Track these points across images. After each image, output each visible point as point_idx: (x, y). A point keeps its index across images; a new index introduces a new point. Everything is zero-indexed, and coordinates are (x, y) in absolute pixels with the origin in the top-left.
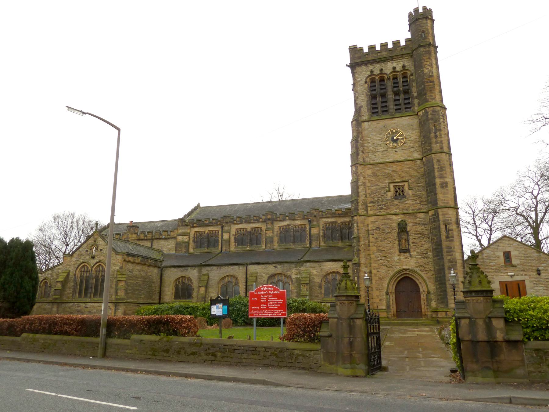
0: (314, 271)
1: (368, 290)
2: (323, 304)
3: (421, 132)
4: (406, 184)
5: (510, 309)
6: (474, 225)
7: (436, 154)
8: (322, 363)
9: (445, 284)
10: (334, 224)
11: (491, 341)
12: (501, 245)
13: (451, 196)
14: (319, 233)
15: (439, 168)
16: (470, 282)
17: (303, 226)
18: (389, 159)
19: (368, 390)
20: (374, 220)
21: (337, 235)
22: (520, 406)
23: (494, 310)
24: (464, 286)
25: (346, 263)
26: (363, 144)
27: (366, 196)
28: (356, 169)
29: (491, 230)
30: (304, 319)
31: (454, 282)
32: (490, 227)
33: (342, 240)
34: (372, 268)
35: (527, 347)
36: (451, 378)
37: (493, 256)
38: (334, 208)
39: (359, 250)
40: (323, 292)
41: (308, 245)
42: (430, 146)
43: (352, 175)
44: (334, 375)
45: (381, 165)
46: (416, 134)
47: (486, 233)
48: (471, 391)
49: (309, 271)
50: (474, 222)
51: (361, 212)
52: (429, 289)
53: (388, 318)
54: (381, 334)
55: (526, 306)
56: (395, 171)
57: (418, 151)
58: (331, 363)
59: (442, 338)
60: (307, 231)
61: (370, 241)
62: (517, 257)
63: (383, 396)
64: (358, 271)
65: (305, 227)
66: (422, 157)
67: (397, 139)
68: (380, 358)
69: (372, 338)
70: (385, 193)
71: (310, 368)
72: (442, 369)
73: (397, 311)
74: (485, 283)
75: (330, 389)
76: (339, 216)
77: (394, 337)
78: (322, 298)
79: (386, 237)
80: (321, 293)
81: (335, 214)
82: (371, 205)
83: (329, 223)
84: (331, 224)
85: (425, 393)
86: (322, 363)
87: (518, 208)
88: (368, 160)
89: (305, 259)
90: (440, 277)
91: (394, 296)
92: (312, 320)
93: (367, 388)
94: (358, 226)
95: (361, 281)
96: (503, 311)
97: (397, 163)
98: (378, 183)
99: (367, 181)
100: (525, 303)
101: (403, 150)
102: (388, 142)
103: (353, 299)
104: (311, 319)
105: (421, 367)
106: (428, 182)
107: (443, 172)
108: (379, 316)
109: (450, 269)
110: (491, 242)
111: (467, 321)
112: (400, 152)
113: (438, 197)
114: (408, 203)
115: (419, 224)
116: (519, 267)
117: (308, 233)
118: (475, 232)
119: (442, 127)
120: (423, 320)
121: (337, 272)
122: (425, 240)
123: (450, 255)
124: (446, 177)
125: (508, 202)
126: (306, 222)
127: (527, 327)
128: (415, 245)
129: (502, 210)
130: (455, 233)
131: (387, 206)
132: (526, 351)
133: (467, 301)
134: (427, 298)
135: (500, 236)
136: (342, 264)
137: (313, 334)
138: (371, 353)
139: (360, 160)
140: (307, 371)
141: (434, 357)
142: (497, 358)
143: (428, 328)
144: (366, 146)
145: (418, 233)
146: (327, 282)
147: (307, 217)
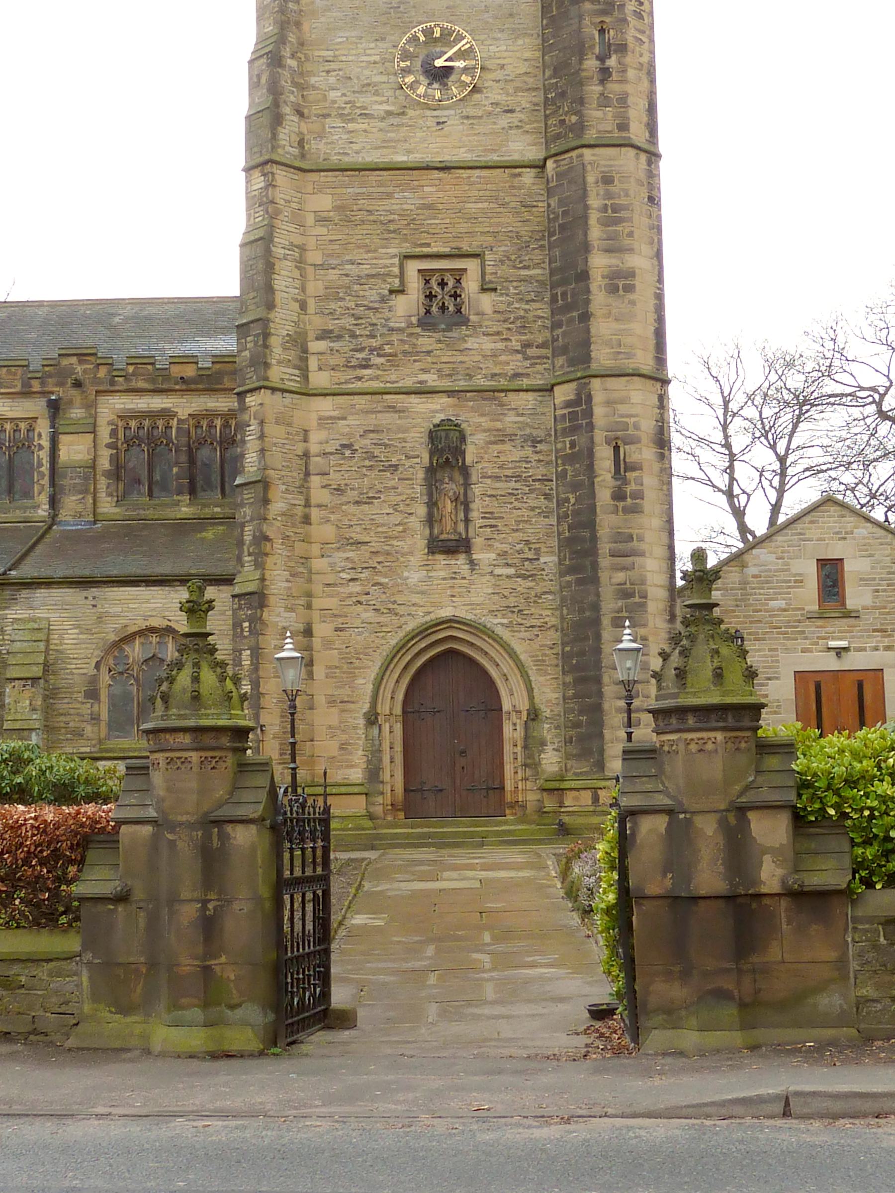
0: (67, 625)
1: (295, 707)
2: (101, 764)
3: (545, 49)
4: (472, 265)
5: (815, 775)
6: (723, 450)
7: (597, 151)
8: (87, 1008)
9: (598, 681)
10: (160, 423)
11: (741, 896)
12: (813, 532)
13: (644, 329)
14: (94, 460)
15: (605, 208)
16: (681, 674)
17: (23, 426)
18: (408, 152)
19: (269, 1106)
20: (335, 413)
21: (175, 470)
22: (817, 1124)
23: (760, 779)
24: (659, 688)
25: (201, 590)
26: (301, 74)
27: (303, 306)
28: (266, 188)
29: (783, 474)
30: (12, 827)
31: (632, 672)
32: (782, 460)
33: (192, 491)
34: (316, 616)
35: (860, 913)
36: (589, 1041)
37: (782, 576)
38: (163, 350)
39: (263, 538)
40: (105, 715)
41: (43, 512)
42: (578, 113)
43: (248, 209)
44: (137, 1052)
45: (373, 177)
46: (528, 54)
47: (766, 483)
48: (657, 1081)
49: (44, 625)
50: (726, 437)
51: (277, 373)
52: (537, 700)
53: (371, 817)
54: (336, 885)
55: (872, 762)
56: (429, 207)
57: (527, 127)
58: (125, 1010)
59: (571, 893)
60: (41, 447)
61: (313, 501)
62: (864, 580)
63: (325, 1124)
64: (257, 625)
65: (31, 429)
66: (542, 155)
67: (448, 71)
68: (325, 978)
69: (298, 898)
70: (383, 300)
71: (35, 1032)
72: (561, 1007)
73: (406, 790)
74: (734, 676)
75: (114, 1111)
76: (184, 387)
77: (390, 893)
78: (100, 742)
79: (379, 487)
80: (95, 719)
81: (167, 378)
82: (321, 346)
83: (141, 416)
84: (146, 423)
85: (491, 1102)
86: (87, 1008)
87: (886, 393)
88: (318, 148)
89: (27, 570)
90: (582, 653)
91: (398, 728)
92: (45, 831)
93: (266, 1099)
94: (262, 437)
95: (267, 669)
96: (791, 783)
97: (441, 175)
98: (358, 255)
99: (311, 243)
100: (869, 752)
101: (468, 117)
102: (410, 79)
103: (225, 741)
104: (42, 828)
105: (485, 1003)
106: (558, 264)
107: (619, 228)
108: (327, 810)
109: (618, 623)
110: (782, 519)
111: (660, 823)
112: (455, 125)
113: (593, 331)
114: (476, 346)
115: (512, 437)
116: (869, 620)
117: (44, 455)
118: (726, 476)
119: (631, 34)
120: (509, 824)
121: (169, 631)
122: (532, 503)
123: (624, 568)
124: (631, 250)
125: (853, 367)
126: (35, 407)
127: (867, 842)
128: (493, 522)
129: (830, 396)
130: (650, 481)
131: (390, 355)
132: (855, 929)
133: (666, 748)
134: (526, 738)
135: (814, 496)
136: (182, 594)
137: (49, 890)
138: (291, 959)
139: (287, 150)
140: (19, 1047)
141: (533, 965)
142: (755, 959)
143: (524, 853)
144: (315, 88)
145: (509, 473)
146: (121, 673)
147: (43, 384)
